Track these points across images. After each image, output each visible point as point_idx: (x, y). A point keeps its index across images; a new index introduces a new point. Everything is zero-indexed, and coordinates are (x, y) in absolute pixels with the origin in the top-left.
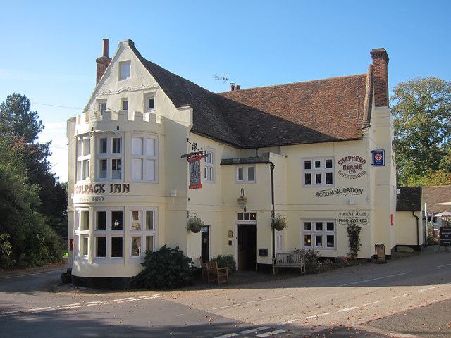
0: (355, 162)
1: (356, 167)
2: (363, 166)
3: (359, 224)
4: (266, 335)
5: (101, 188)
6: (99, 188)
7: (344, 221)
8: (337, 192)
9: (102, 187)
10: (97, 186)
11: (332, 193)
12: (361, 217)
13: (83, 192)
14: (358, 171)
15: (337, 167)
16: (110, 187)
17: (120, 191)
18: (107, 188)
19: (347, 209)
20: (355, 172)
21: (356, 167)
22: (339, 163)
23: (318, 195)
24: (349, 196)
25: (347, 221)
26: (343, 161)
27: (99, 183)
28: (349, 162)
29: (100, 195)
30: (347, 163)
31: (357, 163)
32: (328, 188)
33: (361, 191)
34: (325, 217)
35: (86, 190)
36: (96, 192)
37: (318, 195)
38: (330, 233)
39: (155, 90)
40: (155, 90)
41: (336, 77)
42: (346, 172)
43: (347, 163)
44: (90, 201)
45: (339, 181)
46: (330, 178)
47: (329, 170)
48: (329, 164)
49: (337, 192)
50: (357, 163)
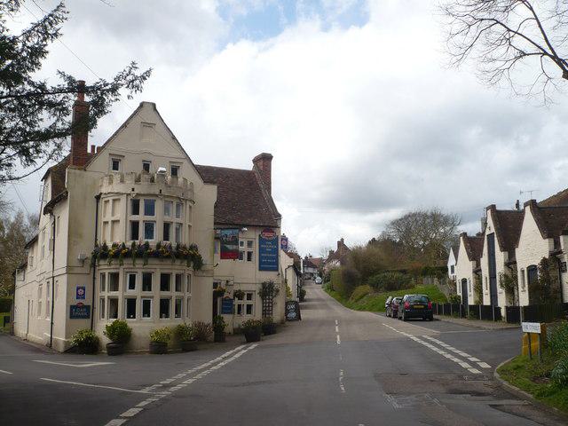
38: (250, 302)
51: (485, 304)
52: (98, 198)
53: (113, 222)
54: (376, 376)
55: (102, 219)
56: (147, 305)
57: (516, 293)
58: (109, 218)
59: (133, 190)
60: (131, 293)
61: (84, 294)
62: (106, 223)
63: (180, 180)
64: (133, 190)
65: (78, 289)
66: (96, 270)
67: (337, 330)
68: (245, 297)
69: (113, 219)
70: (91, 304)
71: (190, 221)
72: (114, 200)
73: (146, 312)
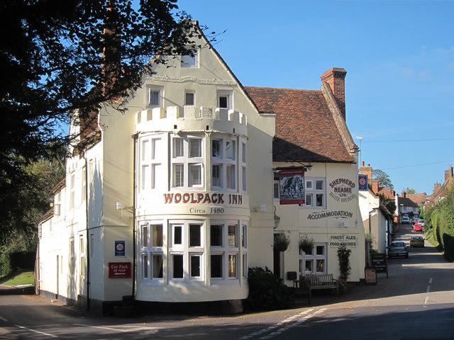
0: (345, 185)
1: (347, 190)
2: (352, 189)
3: (348, 248)
4: (267, 337)
5: (220, 198)
6: (217, 197)
7: (335, 244)
8: (329, 214)
9: (220, 197)
10: (215, 195)
11: (323, 216)
12: (350, 241)
13: (193, 202)
14: (348, 195)
15: (328, 191)
16: (228, 197)
17: (171, 201)
18: (225, 198)
19: (338, 232)
20: (345, 195)
21: (347, 190)
22: (330, 185)
23: (310, 217)
24: (340, 220)
25: (337, 244)
26: (334, 183)
27: (218, 192)
28: (340, 185)
29: (220, 206)
30: (338, 186)
31: (347, 186)
32: (320, 210)
33: (350, 215)
34: (318, 240)
35: (200, 199)
36: (214, 202)
37: (310, 217)
38: (320, 257)
39: (231, 88)
40: (231, 88)
41: (292, 88)
42: (337, 194)
43: (338, 186)
44: (208, 212)
45: (332, 204)
46: (319, 199)
47: (319, 192)
48: (319, 185)
49: (329, 214)
50: (347, 186)
51: (374, 248)
52: (136, 137)
53: (154, 165)
54: (191, 53)
55: (141, 162)
56: (195, 262)
57: (81, 254)
58: (143, 163)
59: (175, 127)
60: (177, 249)
61: (124, 249)
62: (144, 166)
63: (231, 112)
64: (175, 127)
65: (117, 243)
66: (136, 223)
67: (431, 281)
68: (315, 251)
69: (154, 162)
70: (132, 262)
71: (244, 161)
72: (154, 140)
73: (195, 270)
